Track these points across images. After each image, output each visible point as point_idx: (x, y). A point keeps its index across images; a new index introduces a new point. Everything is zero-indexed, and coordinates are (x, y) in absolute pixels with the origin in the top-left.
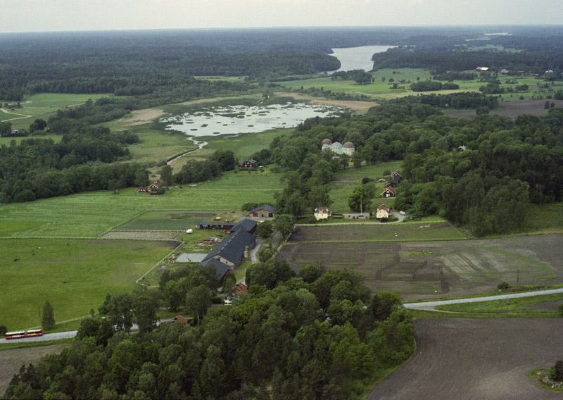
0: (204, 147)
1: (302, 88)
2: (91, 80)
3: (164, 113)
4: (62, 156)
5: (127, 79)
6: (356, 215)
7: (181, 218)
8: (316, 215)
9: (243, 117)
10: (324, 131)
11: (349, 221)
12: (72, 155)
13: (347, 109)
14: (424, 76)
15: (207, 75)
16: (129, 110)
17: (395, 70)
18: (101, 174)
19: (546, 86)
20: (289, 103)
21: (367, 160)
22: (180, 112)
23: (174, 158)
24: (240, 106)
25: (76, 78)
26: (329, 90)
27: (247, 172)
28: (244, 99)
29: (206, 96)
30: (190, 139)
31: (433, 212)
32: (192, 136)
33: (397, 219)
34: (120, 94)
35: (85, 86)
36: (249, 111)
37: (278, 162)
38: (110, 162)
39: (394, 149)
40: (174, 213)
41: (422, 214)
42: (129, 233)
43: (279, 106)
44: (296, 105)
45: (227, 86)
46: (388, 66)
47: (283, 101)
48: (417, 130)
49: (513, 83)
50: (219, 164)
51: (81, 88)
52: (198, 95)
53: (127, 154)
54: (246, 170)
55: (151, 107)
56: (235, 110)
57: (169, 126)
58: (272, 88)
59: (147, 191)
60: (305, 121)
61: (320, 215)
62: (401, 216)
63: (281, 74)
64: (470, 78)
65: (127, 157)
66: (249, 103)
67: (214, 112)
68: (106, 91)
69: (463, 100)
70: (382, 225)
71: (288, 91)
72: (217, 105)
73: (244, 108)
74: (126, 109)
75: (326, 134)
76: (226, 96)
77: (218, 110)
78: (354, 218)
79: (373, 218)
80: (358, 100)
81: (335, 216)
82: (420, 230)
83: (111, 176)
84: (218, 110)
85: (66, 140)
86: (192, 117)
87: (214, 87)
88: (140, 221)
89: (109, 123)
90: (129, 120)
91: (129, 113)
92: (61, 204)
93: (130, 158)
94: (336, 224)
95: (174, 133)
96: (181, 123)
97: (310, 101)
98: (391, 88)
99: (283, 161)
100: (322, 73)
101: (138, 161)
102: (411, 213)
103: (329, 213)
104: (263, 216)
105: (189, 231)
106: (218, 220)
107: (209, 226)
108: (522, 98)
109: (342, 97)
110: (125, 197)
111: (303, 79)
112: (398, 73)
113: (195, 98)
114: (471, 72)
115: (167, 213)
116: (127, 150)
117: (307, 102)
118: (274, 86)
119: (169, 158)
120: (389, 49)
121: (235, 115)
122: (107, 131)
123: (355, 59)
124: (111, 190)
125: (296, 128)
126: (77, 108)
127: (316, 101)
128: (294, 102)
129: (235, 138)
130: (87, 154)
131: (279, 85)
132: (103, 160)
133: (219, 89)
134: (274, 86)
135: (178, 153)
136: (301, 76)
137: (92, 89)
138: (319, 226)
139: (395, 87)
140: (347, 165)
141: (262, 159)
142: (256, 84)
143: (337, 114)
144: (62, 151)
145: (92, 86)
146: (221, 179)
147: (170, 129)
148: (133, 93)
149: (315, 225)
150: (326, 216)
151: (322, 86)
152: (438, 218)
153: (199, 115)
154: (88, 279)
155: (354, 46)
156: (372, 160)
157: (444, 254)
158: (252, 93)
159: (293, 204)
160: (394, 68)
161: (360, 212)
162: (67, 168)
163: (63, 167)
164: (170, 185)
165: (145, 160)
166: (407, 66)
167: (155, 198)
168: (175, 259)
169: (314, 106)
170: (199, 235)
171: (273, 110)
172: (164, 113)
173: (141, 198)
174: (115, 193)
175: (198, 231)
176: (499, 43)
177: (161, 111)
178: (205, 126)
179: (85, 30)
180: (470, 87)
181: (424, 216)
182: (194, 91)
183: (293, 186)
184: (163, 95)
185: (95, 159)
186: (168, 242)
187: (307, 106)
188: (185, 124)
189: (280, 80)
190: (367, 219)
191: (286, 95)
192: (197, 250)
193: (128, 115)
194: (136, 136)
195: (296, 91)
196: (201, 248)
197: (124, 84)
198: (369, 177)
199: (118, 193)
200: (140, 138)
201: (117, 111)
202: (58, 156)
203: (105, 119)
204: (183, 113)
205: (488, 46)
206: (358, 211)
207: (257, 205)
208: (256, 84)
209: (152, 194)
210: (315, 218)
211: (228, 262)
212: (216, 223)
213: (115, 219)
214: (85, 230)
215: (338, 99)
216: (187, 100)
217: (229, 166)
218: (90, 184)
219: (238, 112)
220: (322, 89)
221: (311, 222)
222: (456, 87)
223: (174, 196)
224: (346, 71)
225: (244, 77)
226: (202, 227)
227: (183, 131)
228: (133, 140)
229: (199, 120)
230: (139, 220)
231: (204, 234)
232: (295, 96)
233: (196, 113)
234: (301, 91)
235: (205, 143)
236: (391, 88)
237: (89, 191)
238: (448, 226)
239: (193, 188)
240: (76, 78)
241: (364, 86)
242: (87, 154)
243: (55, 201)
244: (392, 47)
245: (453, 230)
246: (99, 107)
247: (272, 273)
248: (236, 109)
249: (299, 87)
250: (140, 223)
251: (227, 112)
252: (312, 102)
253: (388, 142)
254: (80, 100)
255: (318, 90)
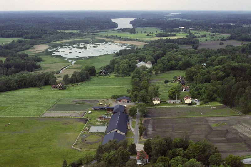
0: (74, 63)
1: (107, 35)
2: (12, 32)
3: (49, 47)
4: (8, 69)
5: (28, 31)
6: (174, 101)
7: (81, 103)
8: (153, 102)
9: (87, 49)
10: (135, 56)
11: (171, 104)
12: (13, 68)
13: (132, 45)
14: (156, 31)
15: (62, 30)
16: (32, 45)
17: (144, 28)
18: (32, 79)
19: (214, 35)
20: (104, 42)
21: (161, 70)
22: (56, 46)
23: (62, 69)
24: (83, 44)
25: (5, 31)
26: (120, 36)
27: (102, 76)
28: (83, 40)
29: (66, 39)
30: (66, 59)
31: (214, 100)
32: (67, 58)
33: (196, 104)
34: (26, 38)
35: (9, 34)
36: (88, 46)
37: (117, 72)
38: (32, 72)
39: (172, 65)
40: (76, 100)
41: (208, 101)
42: (58, 113)
43: (100, 44)
44: (108, 43)
45: (74, 34)
46: (139, 26)
47: (101, 41)
48: (179, 56)
49: (197, 34)
50: (89, 72)
51: (7, 35)
52: (62, 38)
53: (39, 67)
54: (102, 75)
55: (42, 44)
56: (81, 45)
57: (53, 53)
58: (94, 35)
59: (57, 88)
60: (119, 51)
61: (156, 102)
62: (196, 101)
63: (94, 29)
64: (179, 31)
65: (39, 69)
66: (87, 42)
67: (72, 46)
68: (19, 36)
69: (184, 41)
70: (190, 107)
71: (101, 36)
72: (72, 43)
73: (85, 45)
74: (31, 45)
75: (136, 58)
76: (75, 39)
77: (73, 45)
78: (173, 103)
79: (183, 102)
80: (135, 41)
81: (163, 102)
82: (211, 110)
83: (37, 79)
84: (73, 45)
85: (8, 60)
86: (63, 49)
87: (69, 35)
88: (59, 106)
89: (25, 51)
90: (33, 50)
91: (32, 46)
92: (13, 95)
93: (41, 69)
94: (166, 106)
95: (57, 56)
96: (59, 52)
97: (113, 41)
98: (146, 36)
99: (121, 71)
100: (112, 29)
101: (46, 71)
102: (201, 100)
103: (160, 100)
104: (124, 102)
105: (90, 112)
106: (101, 104)
107: (99, 109)
108: (206, 40)
109: (127, 40)
110: (46, 91)
111: (105, 32)
112: (146, 29)
113: (61, 40)
114: (177, 29)
115: (72, 100)
116: (39, 65)
117: (112, 42)
118: (94, 34)
119: (61, 69)
120: (135, 19)
121: (82, 48)
122: (27, 55)
123: (124, 23)
124: (38, 87)
125: (115, 54)
126: (8, 44)
127: (116, 41)
128: (107, 42)
129: (88, 59)
130: (20, 68)
131: (96, 34)
132: (28, 71)
133: (71, 36)
134: (94, 34)
135: (64, 67)
136: (103, 30)
137: (13, 35)
138: (157, 108)
139: (148, 35)
140: (152, 73)
141: (109, 69)
142: (86, 34)
143: (129, 47)
144: (8, 66)
145: (12, 34)
146: (90, 80)
147: (54, 54)
148: (32, 37)
149: (154, 107)
150: (159, 102)
151: (117, 35)
152: (216, 103)
153: (66, 47)
154: (43, 145)
155: (115, 18)
156: (163, 71)
157: (233, 125)
158: (86, 38)
159: (143, 96)
160: (143, 27)
161: (175, 99)
162: (11, 75)
163: (9, 74)
164: (68, 84)
165: (49, 71)
166: (148, 26)
167: (61, 91)
168: (89, 130)
169: (116, 44)
170: (95, 114)
171: (98, 45)
172: (49, 47)
173: (55, 91)
174: (40, 89)
175: (94, 112)
176: (179, 17)
177: (47, 46)
178: (70, 53)
179: (33, 10)
180: (181, 35)
181: (210, 102)
182: (60, 37)
183: (135, 84)
184: (47, 38)
185: (24, 70)
186: (80, 118)
187: (113, 44)
188: (61, 52)
189: (95, 32)
190: (180, 104)
191: (102, 39)
192: (98, 124)
193: (32, 48)
194: (40, 58)
195: (105, 37)
196: (100, 122)
197: (27, 33)
198: (168, 80)
199: (42, 89)
200: (43, 59)
201: (28, 46)
202: (6, 69)
203: (22, 50)
204: (58, 46)
205: (175, 18)
206: (174, 99)
207: (119, 96)
208: (86, 34)
209: (60, 89)
210: (153, 103)
211: (122, 133)
212: (101, 107)
213: (45, 104)
214: (31, 112)
215: (125, 40)
216: (57, 41)
217: (94, 74)
218: (27, 84)
219: (83, 46)
220: (116, 36)
221: (152, 106)
222: (175, 35)
223: (71, 90)
224: (123, 28)
225: (79, 31)
226: (95, 110)
227: (61, 56)
228: (40, 60)
229: (67, 50)
230: (58, 105)
231: (97, 113)
232: (107, 40)
233: (64, 47)
234: (106, 37)
235: (74, 62)
236: (146, 36)
237: (26, 87)
238: (224, 107)
239: (79, 86)
240: (5, 31)
241: (134, 35)
242: (20, 68)
243: (10, 93)
244: (136, 18)
245: (228, 109)
246: (18, 44)
247: (165, 146)
248: (82, 45)
249: (106, 35)
250: (59, 107)
251: (78, 46)
252: (114, 42)
253: (169, 61)
254: (9, 41)
255: (115, 36)
